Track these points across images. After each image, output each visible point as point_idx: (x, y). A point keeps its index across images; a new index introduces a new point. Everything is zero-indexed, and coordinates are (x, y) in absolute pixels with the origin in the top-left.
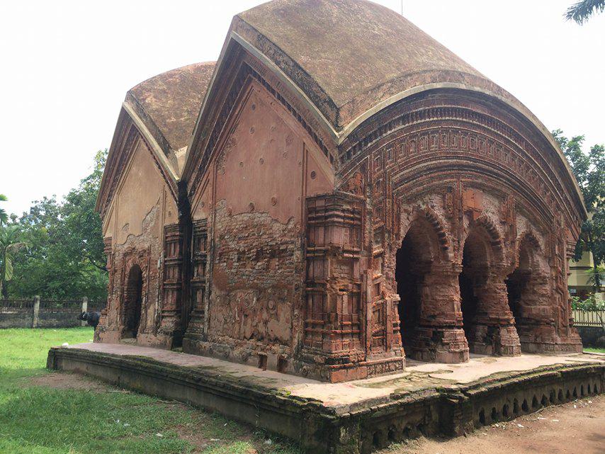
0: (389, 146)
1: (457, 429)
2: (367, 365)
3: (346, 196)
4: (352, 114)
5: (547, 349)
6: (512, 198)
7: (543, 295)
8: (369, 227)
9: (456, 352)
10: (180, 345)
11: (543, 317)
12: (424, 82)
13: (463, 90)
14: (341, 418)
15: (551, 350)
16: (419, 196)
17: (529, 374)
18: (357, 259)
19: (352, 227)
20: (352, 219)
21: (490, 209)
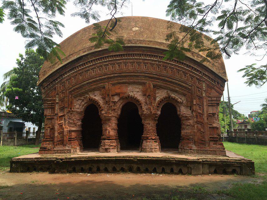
0: (67, 80)
1: (56, 171)
2: (54, 150)
3: (47, 99)
4: (44, 75)
5: (185, 152)
6: (150, 84)
7: (188, 125)
8: (57, 107)
9: (103, 149)
10: (142, 151)
11: (186, 136)
12: (164, 47)
13: (141, 46)
14: (13, 161)
15: (187, 152)
16: (87, 92)
17: (111, 157)
18: (53, 118)
19: (52, 108)
20: (51, 106)
21: (135, 92)
